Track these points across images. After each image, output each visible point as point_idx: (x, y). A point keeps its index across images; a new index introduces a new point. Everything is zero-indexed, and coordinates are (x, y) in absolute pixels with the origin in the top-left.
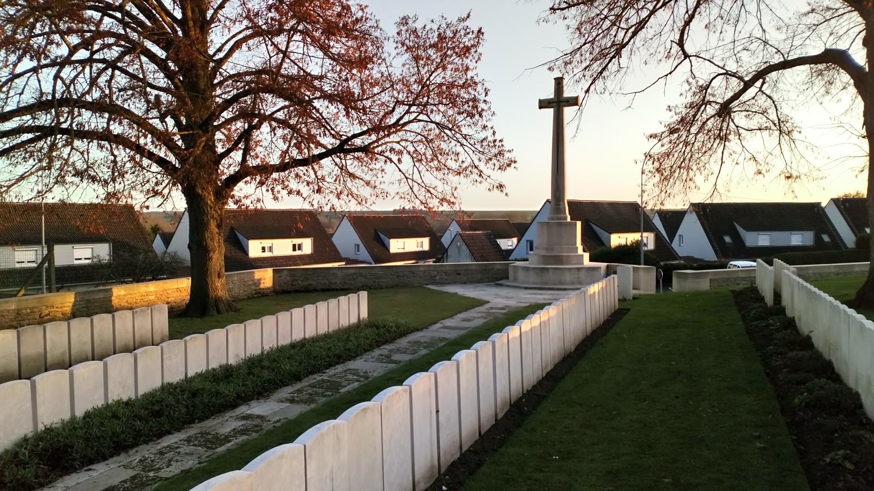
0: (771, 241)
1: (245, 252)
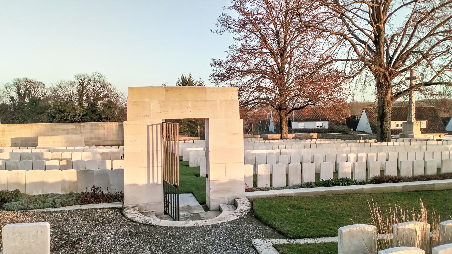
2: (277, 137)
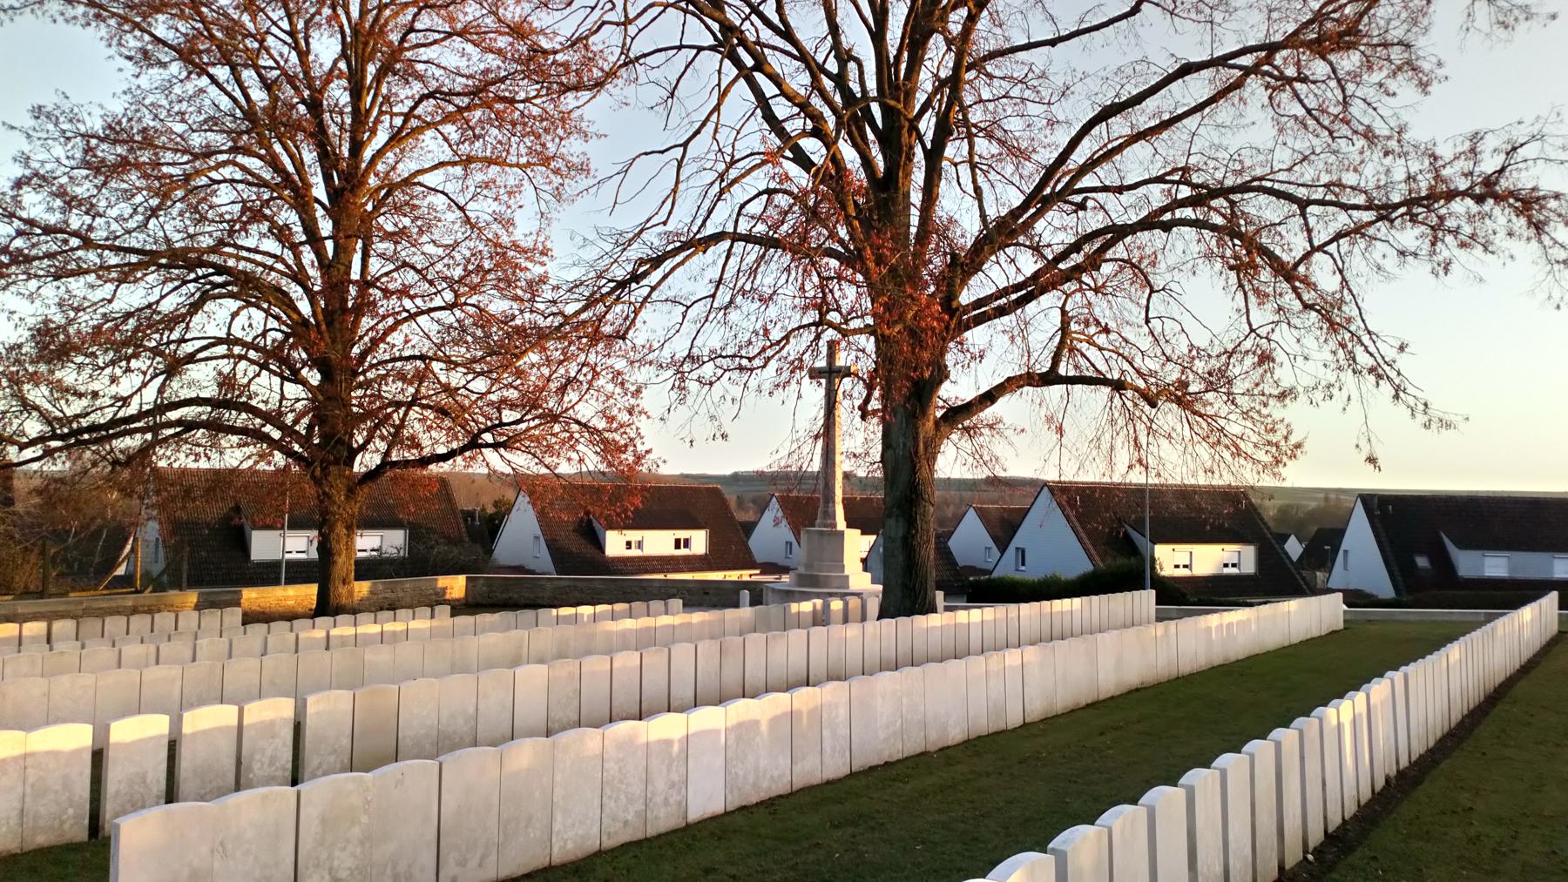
0: (1511, 569)
1: (600, 546)
2: (287, 598)
